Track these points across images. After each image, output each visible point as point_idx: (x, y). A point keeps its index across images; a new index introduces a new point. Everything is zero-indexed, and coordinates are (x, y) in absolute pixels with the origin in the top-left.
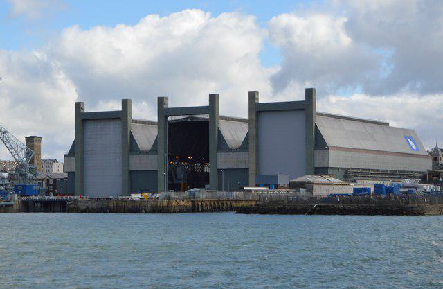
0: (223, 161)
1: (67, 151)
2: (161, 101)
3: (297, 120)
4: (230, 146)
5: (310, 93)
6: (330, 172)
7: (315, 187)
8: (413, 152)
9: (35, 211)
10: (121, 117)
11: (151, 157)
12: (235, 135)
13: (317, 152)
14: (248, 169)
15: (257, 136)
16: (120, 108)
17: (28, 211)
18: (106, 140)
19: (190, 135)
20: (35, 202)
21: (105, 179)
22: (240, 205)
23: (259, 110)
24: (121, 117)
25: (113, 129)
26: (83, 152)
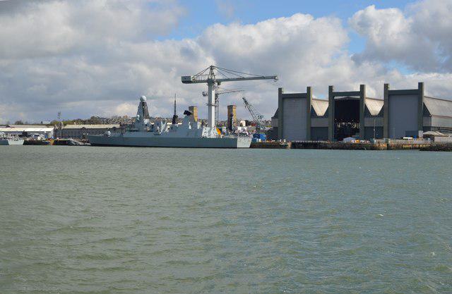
0: (368, 123)
1: (273, 115)
2: (280, 90)
3: (413, 101)
4: (373, 113)
5: (362, 87)
6: (432, 129)
7: (435, 137)
10: (306, 97)
12: (375, 107)
13: (425, 118)
14: (383, 127)
16: (416, 87)
17: (295, 148)
19: (347, 107)
20: (299, 143)
21: (297, 128)
22: (407, 146)
23: (390, 96)
24: (306, 97)
25: (301, 103)
26: (282, 116)
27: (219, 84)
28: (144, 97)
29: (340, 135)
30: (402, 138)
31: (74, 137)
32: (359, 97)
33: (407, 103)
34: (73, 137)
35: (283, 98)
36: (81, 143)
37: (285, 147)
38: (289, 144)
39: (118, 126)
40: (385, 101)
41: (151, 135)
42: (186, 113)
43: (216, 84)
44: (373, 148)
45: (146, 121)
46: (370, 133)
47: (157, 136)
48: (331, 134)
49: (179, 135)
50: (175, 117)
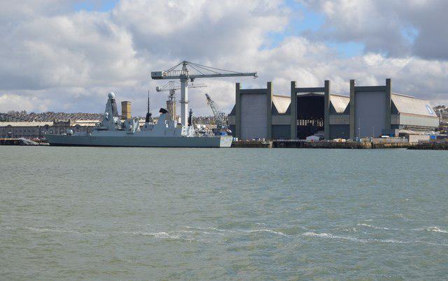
0: (333, 121)
2: (293, 84)
3: (381, 96)
4: (338, 111)
8: (430, 115)
9: (280, 147)
10: (266, 93)
11: (286, 117)
13: (392, 116)
15: (355, 106)
16: (266, 87)
18: (255, 107)
19: (311, 104)
20: (280, 142)
21: (255, 124)
22: (388, 145)
23: (357, 92)
24: (266, 93)
25: (261, 100)
27: (192, 81)
28: (113, 94)
29: (304, 132)
30: (380, 137)
31: (27, 137)
32: (323, 93)
33: (375, 101)
34: (25, 136)
35: (241, 94)
36: (35, 143)
37: (267, 146)
38: (271, 143)
39: (51, 124)
40: (351, 98)
41: (123, 134)
42: (162, 111)
43: (190, 80)
44: (360, 147)
45: (116, 119)
46: (343, 130)
47: (130, 136)
48: (294, 132)
49: (155, 134)
50: (149, 115)
